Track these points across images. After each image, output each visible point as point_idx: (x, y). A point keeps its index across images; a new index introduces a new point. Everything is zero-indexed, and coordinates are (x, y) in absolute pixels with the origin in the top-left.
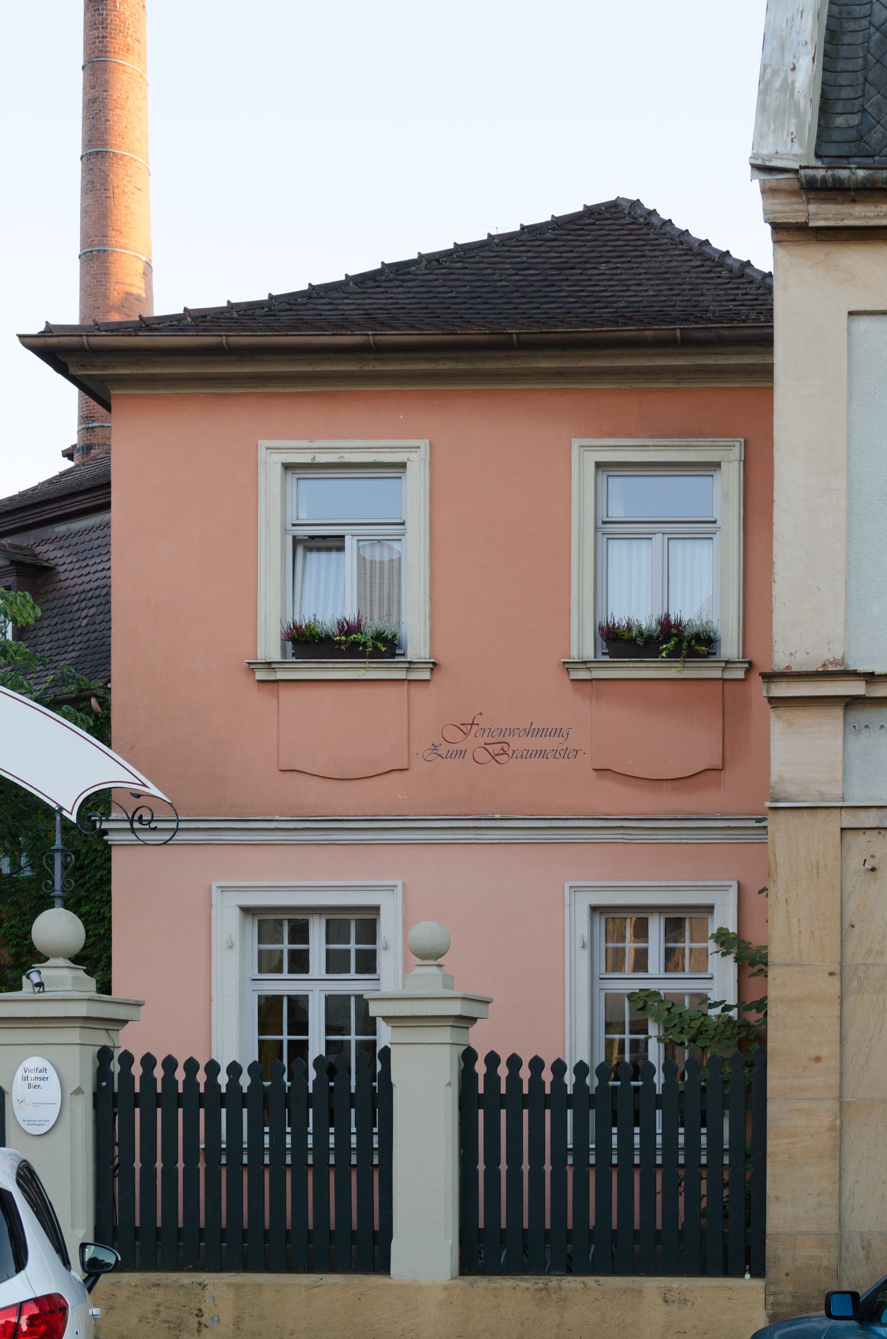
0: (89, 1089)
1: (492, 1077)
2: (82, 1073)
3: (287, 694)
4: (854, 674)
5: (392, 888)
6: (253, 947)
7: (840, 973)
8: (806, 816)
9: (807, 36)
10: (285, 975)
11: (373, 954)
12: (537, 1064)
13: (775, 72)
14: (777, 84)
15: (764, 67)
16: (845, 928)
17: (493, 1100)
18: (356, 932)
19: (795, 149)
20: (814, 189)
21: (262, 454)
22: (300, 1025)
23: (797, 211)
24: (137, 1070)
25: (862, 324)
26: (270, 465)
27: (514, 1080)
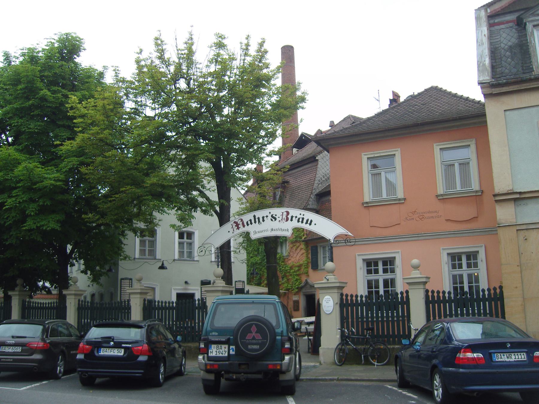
0: (339, 303)
1: (433, 296)
2: (337, 300)
3: (371, 209)
4: (517, 193)
5: (398, 252)
6: (366, 268)
7: (520, 265)
8: (508, 228)
9: (487, 54)
10: (389, 274)
11: (477, 263)
12: (438, 292)
13: (480, 62)
14: (481, 65)
15: (478, 62)
16: (520, 254)
17: (433, 302)
18: (389, 264)
19: (487, 78)
20: (492, 86)
21: (363, 156)
22: (377, 287)
23: (489, 91)
24: (349, 298)
25: (508, 113)
26: (365, 158)
27: (438, 296)
